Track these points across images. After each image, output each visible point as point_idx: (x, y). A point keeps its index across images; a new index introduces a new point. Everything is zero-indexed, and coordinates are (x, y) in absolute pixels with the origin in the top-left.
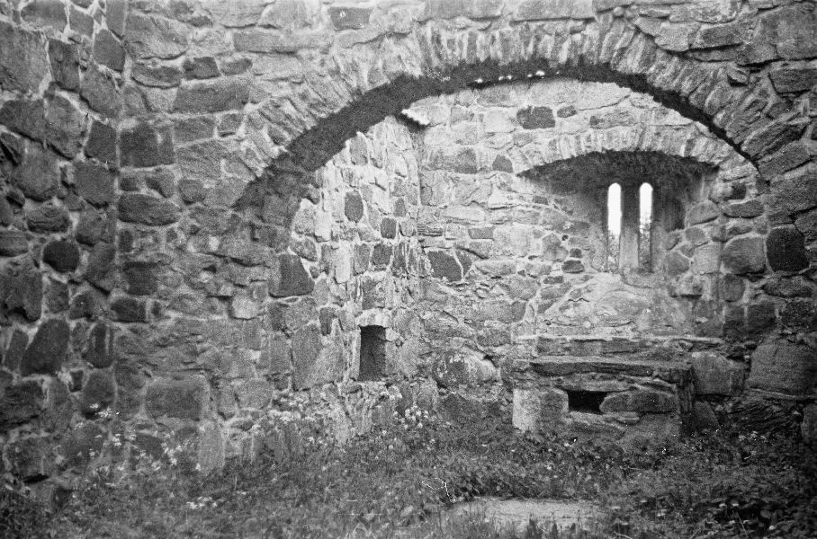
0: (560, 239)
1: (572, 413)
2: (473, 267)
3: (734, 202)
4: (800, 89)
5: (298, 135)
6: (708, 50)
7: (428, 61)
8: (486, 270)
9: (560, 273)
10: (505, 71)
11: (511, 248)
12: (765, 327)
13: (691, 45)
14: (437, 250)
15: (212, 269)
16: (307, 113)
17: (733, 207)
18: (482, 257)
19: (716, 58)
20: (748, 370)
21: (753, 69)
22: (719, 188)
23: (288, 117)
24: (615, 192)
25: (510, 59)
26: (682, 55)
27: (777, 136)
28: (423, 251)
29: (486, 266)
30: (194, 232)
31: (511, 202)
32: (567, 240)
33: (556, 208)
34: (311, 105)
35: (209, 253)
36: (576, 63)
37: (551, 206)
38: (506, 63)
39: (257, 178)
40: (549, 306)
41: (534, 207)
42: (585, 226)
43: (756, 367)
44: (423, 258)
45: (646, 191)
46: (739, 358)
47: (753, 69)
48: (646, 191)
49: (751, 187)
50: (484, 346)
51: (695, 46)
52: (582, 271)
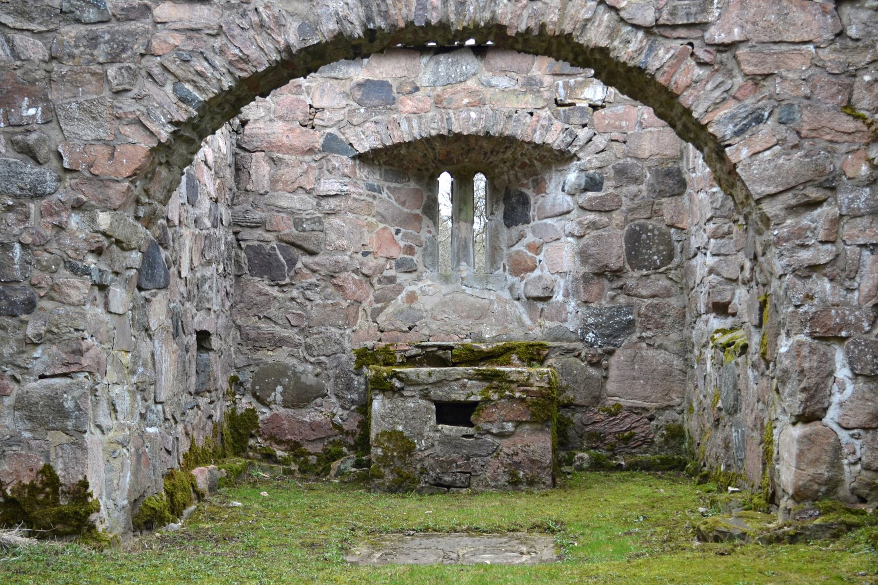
0: (394, 233)
1: (440, 426)
2: (299, 265)
3: (590, 194)
4: (766, 72)
5: (212, 95)
6: (675, 27)
7: (369, 19)
8: (315, 267)
9: (392, 273)
10: (466, 33)
11: (345, 242)
12: (624, 329)
13: (657, 20)
14: (256, 243)
15: (98, 252)
16: (225, 71)
17: (590, 200)
18: (312, 253)
19: (682, 36)
20: (606, 378)
21: (721, 48)
22: (572, 176)
23: (200, 74)
24: (445, 180)
25: (465, 24)
26: (647, 30)
27: (744, 118)
28: (240, 246)
29: (317, 264)
30: (78, 206)
31: (345, 188)
32: (400, 235)
33: (391, 198)
34: (231, 63)
35: (97, 232)
36: (536, 32)
37: (384, 195)
38: (460, 28)
39: (160, 143)
40: (381, 310)
41: (368, 195)
42: (417, 218)
43: (613, 373)
44: (239, 252)
45: (480, 181)
46: (596, 365)
47: (721, 48)
48: (480, 181)
49: (609, 179)
50: (314, 356)
51: (661, 21)
52: (415, 271)
